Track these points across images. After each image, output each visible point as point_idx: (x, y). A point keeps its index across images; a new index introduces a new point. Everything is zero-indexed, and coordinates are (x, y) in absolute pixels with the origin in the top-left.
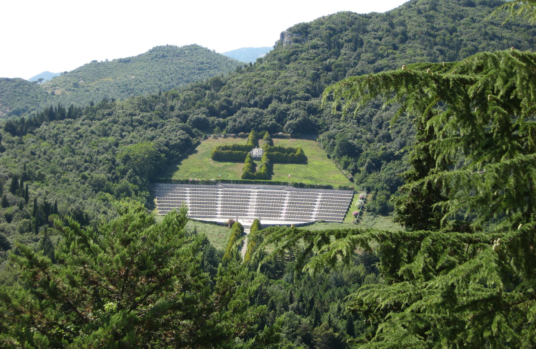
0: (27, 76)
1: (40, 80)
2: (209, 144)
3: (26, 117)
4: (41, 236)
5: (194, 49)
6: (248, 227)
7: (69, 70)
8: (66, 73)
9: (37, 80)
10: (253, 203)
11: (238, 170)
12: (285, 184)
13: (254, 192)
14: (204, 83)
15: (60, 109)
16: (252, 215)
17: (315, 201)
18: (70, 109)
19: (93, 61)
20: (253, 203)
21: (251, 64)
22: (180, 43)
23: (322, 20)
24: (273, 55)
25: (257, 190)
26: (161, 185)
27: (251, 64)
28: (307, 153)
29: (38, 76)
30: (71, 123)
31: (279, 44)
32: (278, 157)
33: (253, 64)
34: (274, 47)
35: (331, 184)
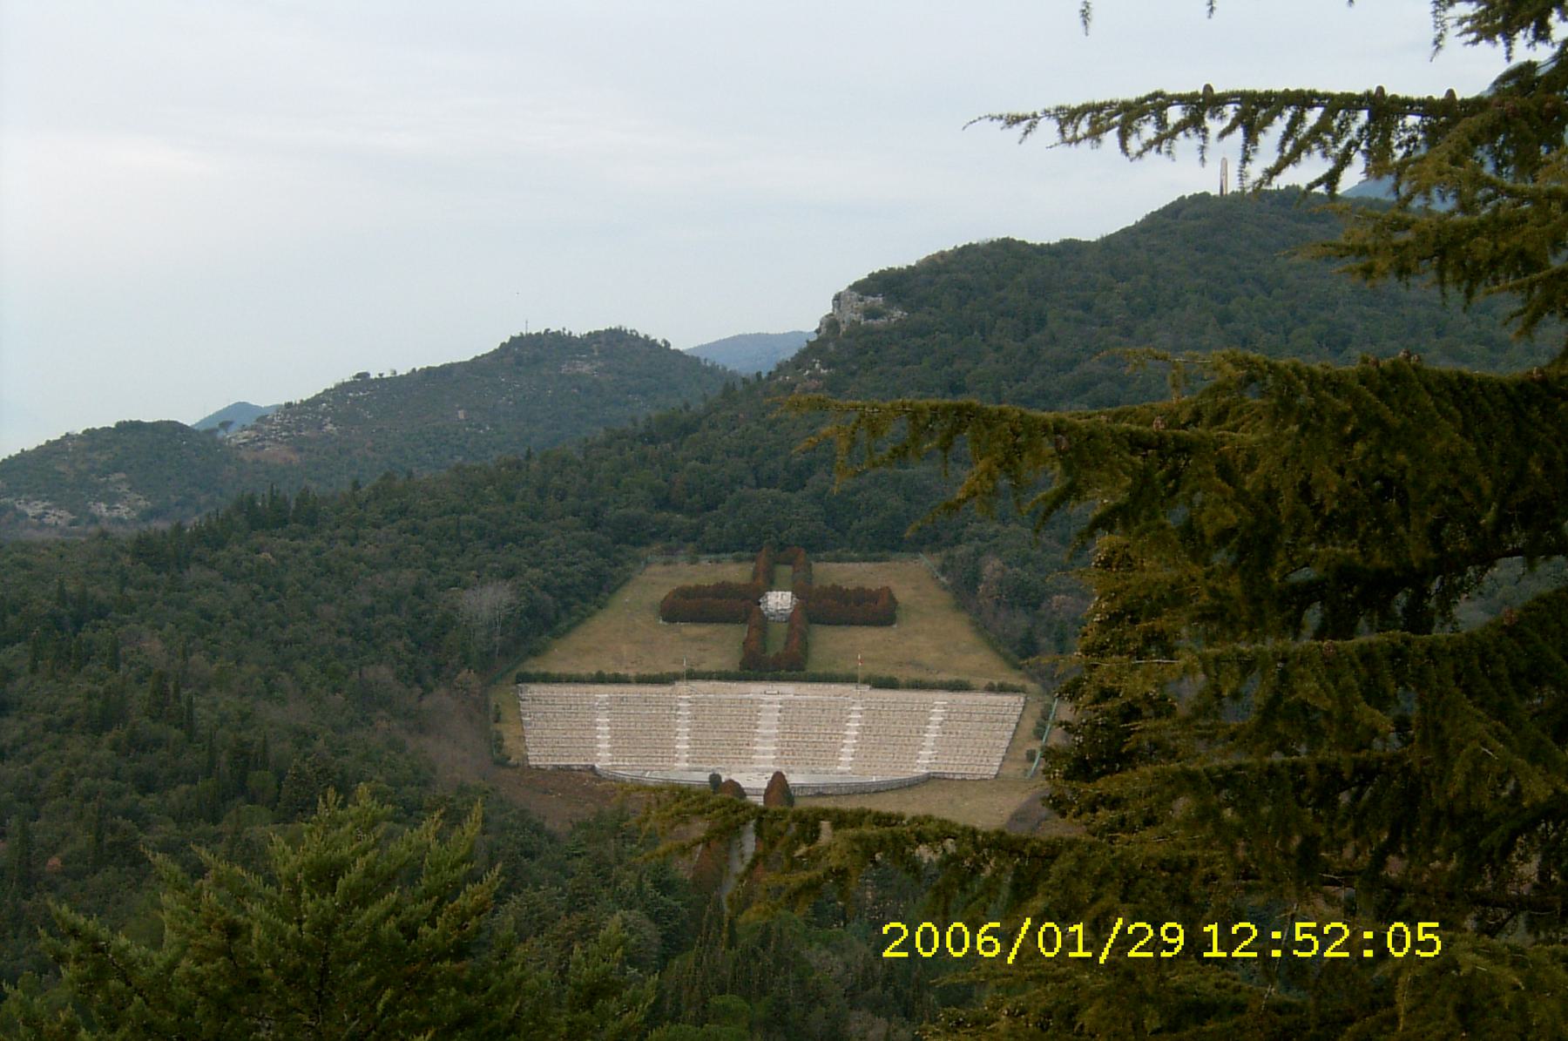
0: (190, 415)
1: (225, 425)
2: (660, 577)
3: (193, 521)
4: (225, 826)
5: (615, 343)
6: (756, 792)
7: (296, 400)
8: (289, 405)
9: (217, 425)
10: (769, 724)
11: (724, 643)
12: (850, 679)
13: (771, 697)
14: (641, 428)
15: (274, 498)
16: (765, 761)
17: (918, 732)
18: (302, 500)
19: (358, 376)
20: (769, 724)
21: (759, 375)
22: (56, 436)
23: (940, 261)
24: (815, 349)
25: (780, 697)
26: (535, 689)
27: (759, 375)
28: (903, 594)
29: (219, 414)
30: (303, 536)
31: (831, 324)
32: (830, 609)
33: (764, 376)
34: (818, 331)
35: (964, 678)
